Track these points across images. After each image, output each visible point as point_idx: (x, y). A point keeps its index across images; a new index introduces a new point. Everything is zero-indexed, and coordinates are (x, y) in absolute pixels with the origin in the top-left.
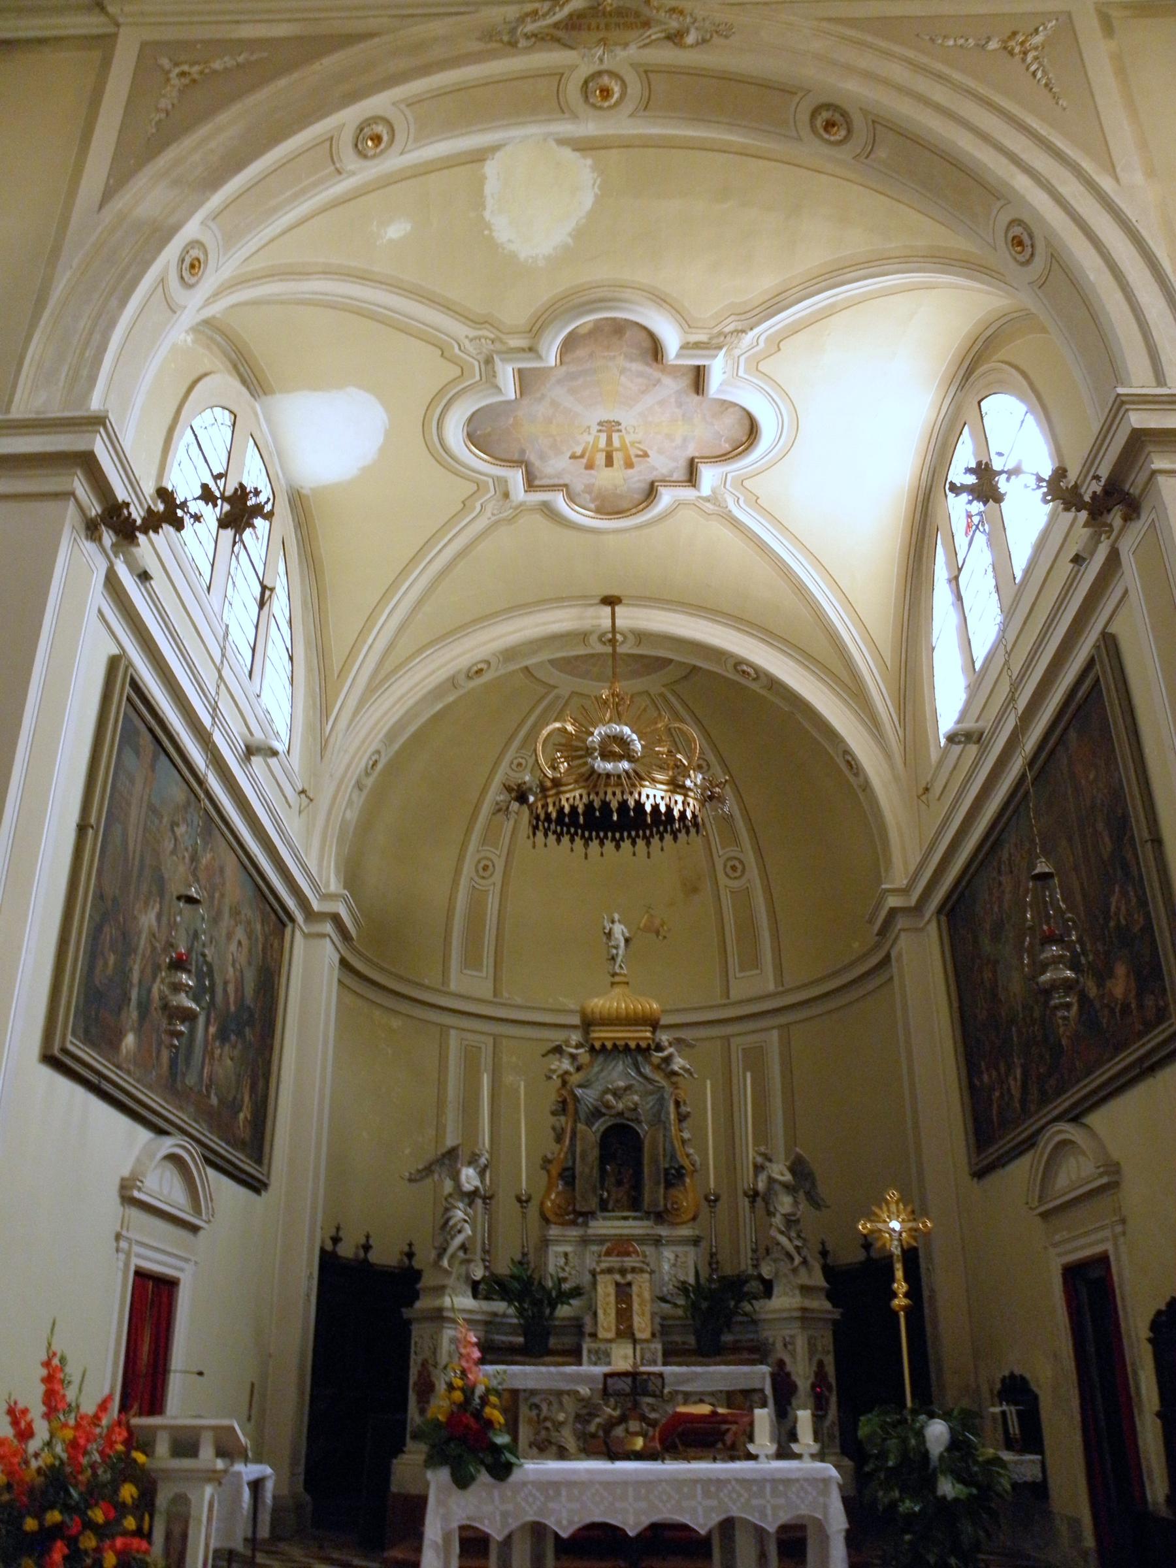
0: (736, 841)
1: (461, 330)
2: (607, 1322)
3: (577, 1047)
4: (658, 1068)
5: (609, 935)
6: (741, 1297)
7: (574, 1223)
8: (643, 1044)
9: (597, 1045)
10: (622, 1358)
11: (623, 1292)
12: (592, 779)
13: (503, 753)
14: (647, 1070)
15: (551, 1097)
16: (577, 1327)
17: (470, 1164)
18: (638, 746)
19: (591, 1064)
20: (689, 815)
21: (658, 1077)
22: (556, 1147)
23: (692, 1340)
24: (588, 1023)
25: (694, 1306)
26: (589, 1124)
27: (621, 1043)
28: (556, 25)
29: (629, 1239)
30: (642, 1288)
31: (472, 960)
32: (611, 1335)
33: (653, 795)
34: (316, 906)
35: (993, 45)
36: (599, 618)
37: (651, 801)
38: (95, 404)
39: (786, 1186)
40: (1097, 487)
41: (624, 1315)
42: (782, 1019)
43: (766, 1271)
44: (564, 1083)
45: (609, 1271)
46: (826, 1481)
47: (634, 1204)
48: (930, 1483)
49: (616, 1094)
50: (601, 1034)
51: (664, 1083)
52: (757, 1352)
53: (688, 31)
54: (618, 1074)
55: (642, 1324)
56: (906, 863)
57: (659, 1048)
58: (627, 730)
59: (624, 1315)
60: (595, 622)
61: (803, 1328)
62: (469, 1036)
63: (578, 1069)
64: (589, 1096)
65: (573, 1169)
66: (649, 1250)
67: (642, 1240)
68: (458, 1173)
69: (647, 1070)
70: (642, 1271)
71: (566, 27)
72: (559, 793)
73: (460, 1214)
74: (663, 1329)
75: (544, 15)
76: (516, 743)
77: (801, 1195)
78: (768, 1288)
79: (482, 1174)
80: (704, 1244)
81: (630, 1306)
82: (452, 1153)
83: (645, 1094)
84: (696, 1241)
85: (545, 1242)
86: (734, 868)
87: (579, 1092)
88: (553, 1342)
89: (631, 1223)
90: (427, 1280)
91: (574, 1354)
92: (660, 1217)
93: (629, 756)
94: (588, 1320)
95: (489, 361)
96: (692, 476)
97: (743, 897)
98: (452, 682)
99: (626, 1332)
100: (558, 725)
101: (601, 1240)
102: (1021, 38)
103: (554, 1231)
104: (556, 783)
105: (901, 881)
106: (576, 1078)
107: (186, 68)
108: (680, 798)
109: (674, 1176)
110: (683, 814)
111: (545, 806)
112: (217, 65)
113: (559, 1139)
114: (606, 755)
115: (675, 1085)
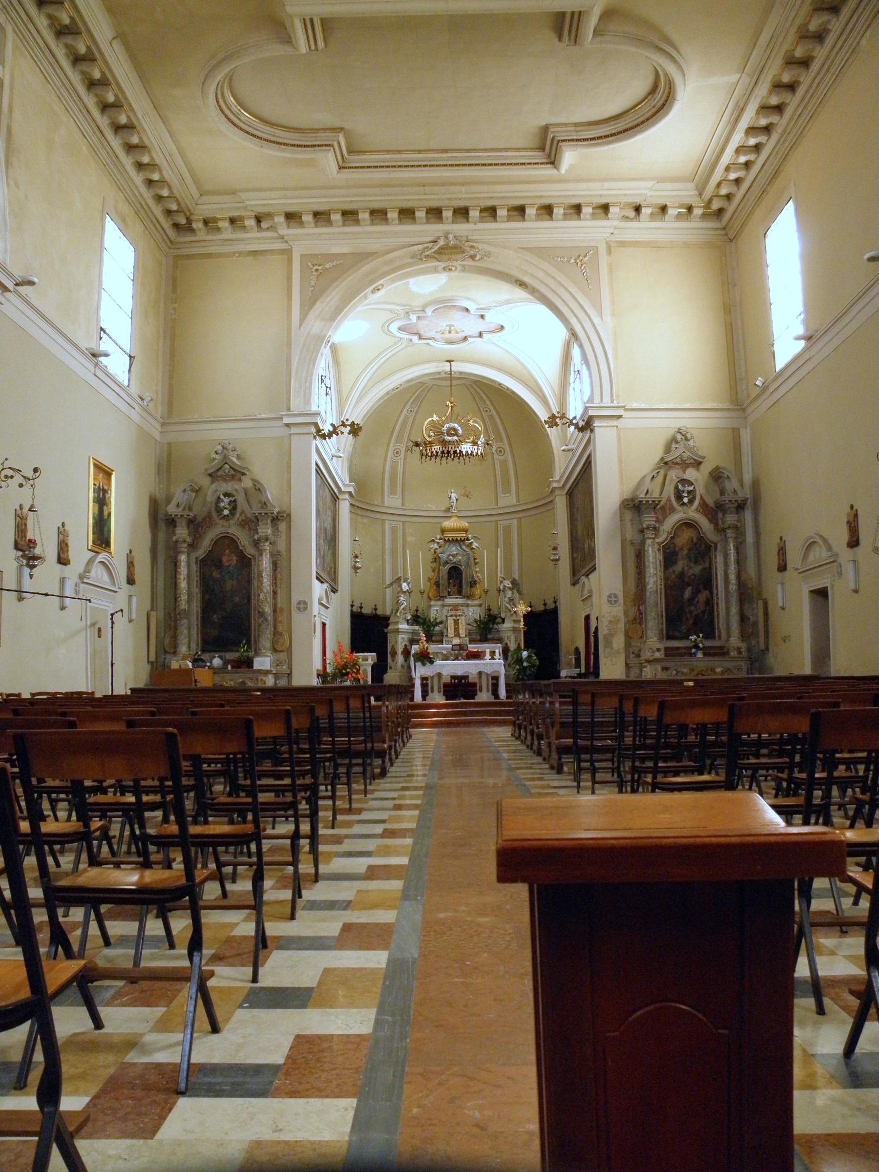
0: (501, 440)
1: (398, 308)
2: (451, 632)
3: (440, 539)
4: (468, 546)
5: (450, 498)
6: (494, 623)
7: (439, 600)
8: (463, 538)
9: (447, 539)
10: (456, 641)
11: (456, 622)
12: (444, 443)
13: (404, 407)
14: (464, 547)
15: (430, 556)
16: (441, 634)
17: (405, 582)
18: (460, 431)
19: (444, 545)
20: (479, 454)
21: (468, 550)
22: (433, 574)
23: (479, 637)
24: (443, 531)
25: (479, 626)
26: (444, 566)
27: (455, 538)
28: (434, 252)
29: (458, 605)
30: (462, 622)
31: (393, 491)
32: (453, 636)
33: (466, 448)
34: (343, 490)
35: (572, 261)
36: (444, 366)
37: (465, 450)
38: (314, 408)
39: (510, 588)
40: (583, 423)
41: (457, 630)
42: (517, 516)
43: (503, 616)
44: (435, 552)
45: (452, 616)
46: (501, 664)
47: (460, 592)
48: (522, 663)
49: (454, 556)
50: (448, 535)
51: (469, 552)
52: (499, 640)
53: (476, 256)
54: (454, 549)
55: (462, 632)
56: (560, 469)
57: (468, 539)
58: (456, 426)
59: (457, 630)
60: (443, 369)
61: (514, 633)
62: (394, 523)
63: (440, 547)
64: (444, 557)
65: (438, 582)
66: (465, 608)
67: (462, 605)
68: (401, 585)
69: (464, 547)
70: (462, 615)
71: (438, 253)
72: (431, 446)
73: (402, 599)
74: (469, 634)
75: (431, 248)
76: (410, 403)
77: (515, 591)
78: (503, 620)
79: (408, 584)
80: (483, 606)
81: (458, 627)
82: (399, 579)
83: (463, 555)
84: (480, 605)
85: (430, 606)
86: (500, 451)
87: (440, 555)
88: (433, 638)
89: (458, 599)
90: (392, 620)
91: (441, 642)
92: (468, 597)
93: (456, 434)
94: (445, 631)
95: (407, 313)
96: (480, 335)
97: (504, 463)
98: (388, 393)
99: (457, 635)
100: (430, 419)
101: (449, 605)
102: (581, 258)
103: (433, 602)
104: (430, 443)
105: (557, 478)
106: (439, 550)
107: (317, 267)
108: (476, 447)
109: (473, 584)
110: (477, 454)
111: (426, 450)
112: (327, 266)
113: (433, 571)
114: (449, 434)
115: (474, 553)
